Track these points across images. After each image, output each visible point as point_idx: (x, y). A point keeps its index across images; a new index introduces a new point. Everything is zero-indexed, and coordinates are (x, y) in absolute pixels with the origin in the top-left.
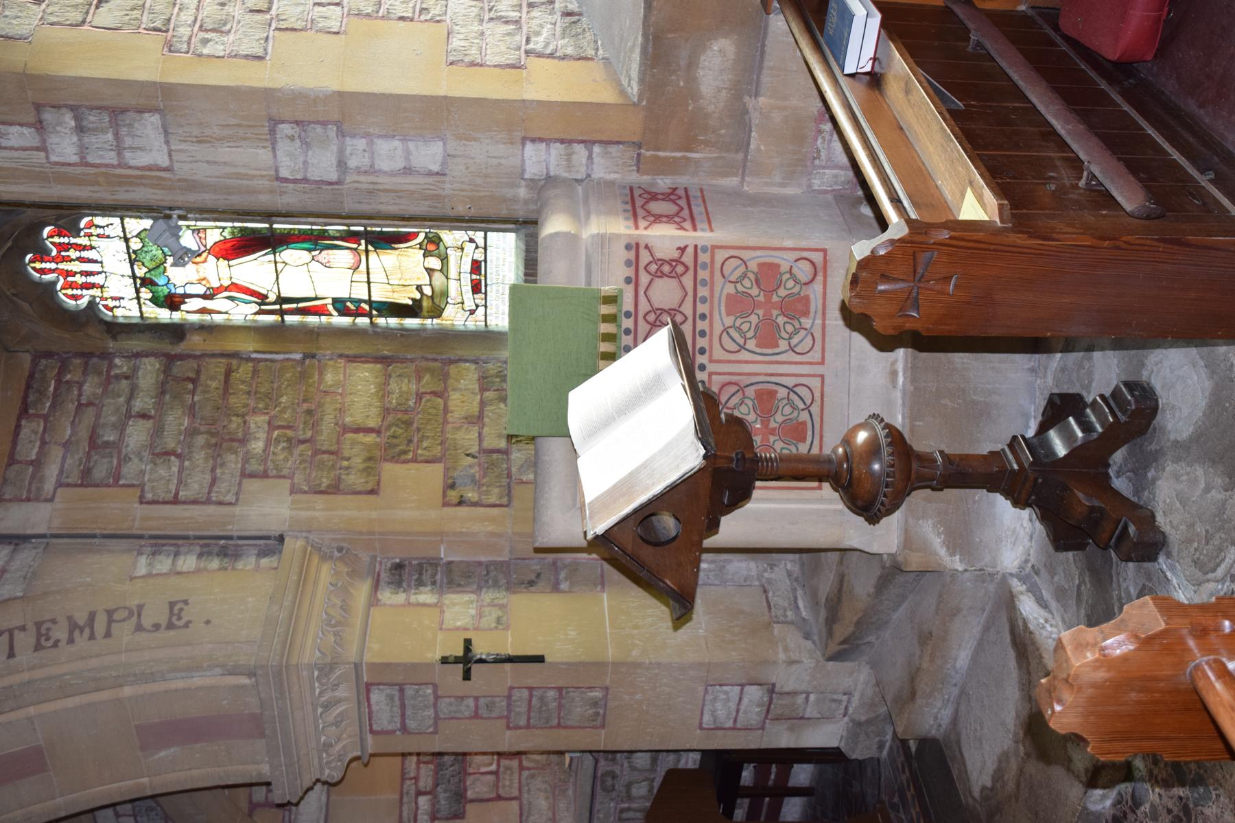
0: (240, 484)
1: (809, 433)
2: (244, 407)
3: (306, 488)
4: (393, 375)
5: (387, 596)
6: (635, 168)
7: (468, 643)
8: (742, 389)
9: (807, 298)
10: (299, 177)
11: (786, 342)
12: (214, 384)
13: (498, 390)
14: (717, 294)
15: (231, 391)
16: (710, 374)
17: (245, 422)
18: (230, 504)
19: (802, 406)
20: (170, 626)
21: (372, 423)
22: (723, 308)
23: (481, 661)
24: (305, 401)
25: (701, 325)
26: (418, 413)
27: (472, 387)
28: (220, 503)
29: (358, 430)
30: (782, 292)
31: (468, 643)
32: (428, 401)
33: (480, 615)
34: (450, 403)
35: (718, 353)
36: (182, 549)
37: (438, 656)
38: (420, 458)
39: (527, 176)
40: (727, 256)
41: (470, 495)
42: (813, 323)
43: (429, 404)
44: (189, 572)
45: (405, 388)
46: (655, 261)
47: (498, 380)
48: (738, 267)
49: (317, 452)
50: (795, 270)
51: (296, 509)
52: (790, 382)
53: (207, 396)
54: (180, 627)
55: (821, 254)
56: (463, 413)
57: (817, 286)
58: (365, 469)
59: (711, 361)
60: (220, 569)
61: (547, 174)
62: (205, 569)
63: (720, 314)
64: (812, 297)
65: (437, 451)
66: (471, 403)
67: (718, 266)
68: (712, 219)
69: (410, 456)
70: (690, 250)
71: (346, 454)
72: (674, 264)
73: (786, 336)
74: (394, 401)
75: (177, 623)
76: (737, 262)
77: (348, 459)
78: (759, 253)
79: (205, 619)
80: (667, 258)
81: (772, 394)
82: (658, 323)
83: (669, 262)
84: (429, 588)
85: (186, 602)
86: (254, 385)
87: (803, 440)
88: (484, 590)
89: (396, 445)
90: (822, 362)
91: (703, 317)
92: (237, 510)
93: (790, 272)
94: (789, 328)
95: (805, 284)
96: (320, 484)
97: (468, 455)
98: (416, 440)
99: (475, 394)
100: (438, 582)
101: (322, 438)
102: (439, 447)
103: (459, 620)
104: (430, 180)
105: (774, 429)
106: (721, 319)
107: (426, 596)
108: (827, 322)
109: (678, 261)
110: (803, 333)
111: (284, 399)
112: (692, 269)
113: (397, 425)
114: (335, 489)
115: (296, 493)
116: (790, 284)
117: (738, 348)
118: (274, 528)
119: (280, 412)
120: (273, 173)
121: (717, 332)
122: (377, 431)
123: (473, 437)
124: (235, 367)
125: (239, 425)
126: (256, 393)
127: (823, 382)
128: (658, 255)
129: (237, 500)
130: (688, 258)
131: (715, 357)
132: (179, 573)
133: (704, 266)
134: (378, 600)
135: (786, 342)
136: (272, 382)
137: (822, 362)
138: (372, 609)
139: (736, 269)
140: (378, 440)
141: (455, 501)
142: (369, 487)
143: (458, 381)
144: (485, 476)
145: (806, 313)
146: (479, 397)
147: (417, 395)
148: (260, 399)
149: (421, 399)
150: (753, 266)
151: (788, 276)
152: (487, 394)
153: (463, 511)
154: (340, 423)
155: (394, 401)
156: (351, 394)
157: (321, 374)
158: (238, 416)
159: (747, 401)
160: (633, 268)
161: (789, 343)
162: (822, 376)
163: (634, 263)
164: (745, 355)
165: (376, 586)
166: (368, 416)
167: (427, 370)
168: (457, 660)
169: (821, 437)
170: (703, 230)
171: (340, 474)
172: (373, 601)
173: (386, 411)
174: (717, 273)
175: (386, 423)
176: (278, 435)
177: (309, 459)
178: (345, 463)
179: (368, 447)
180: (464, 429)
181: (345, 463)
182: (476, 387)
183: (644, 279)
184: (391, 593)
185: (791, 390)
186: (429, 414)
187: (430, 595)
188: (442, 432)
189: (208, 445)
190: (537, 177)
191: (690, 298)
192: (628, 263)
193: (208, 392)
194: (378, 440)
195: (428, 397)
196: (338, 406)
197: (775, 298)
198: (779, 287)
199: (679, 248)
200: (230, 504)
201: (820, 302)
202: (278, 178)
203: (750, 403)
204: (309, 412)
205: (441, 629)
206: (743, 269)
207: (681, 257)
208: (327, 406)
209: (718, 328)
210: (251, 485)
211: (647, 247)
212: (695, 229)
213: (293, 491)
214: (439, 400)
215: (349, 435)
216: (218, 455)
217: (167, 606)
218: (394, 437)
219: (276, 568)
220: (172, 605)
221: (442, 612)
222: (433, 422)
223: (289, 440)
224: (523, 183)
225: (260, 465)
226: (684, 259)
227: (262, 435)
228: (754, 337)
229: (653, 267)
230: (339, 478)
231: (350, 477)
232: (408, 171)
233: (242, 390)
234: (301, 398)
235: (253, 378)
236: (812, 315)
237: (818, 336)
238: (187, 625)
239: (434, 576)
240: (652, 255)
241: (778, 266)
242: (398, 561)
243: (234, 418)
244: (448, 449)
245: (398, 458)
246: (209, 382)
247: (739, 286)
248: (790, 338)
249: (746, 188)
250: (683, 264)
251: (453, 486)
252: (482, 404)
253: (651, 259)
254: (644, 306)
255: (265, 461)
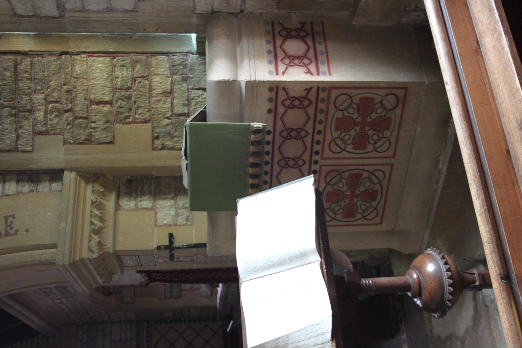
0: (33, 139)
1: (379, 196)
2: (28, 89)
3: (72, 141)
4: (117, 66)
5: (127, 203)
6: (276, 7)
7: (171, 236)
8: (340, 173)
9: (390, 119)
10: (31, 14)
11: (372, 146)
12: (8, 74)
13: (182, 74)
14: (330, 118)
15: (19, 78)
16: (321, 166)
17: (31, 99)
18: (30, 152)
19: (377, 181)
20: (7, 234)
21: (107, 98)
22: (333, 127)
23: (179, 248)
24: (65, 84)
25: (317, 137)
26: (134, 91)
27: (166, 73)
28: (24, 151)
29: (99, 103)
30: (374, 116)
31: (171, 236)
32: (140, 82)
33: (177, 215)
34: (153, 84)
35: (327, 153)
36: (7, 177)
37: (155, 246)
38: (138, 121)
39: (197, 12)
40: (339, 93)
41: (168, 143)
42: (391, 134)
43: (140, 85)
44: (13, 195)
45: (125, 75)
46: (289, 98)
47: (181, 67)
48: (346, 100)
49: (76, 118)
50: (384, 102)
51: (67, 154)
52: (371, 169)
53: (5, 82)
54: (12, 235)
55: (404, 91)
56: (161, 91)
57: (398, 112)
58: (105, 129)
59: (322, 158)
60: (30, 192)
61: (212, 10)
62: (22, 193)
63: (331, 130)
64: (393, 117)
65: (147, 116)
66: (166, 83)
67: (332, 100)
68: (330, 59)
69: (131, 119)
70: (314, 90)
71: (93, 119)
72: (302, 99)
73: (373, 142)
74: (119, 83)
75: (10, 231)
76: (345, 97)
77: (95, 122)
78: (361, 91)
79: (25, 229)
80: (298, 95)
81: (359, 176)
82: (289, 137)
83: (299, 99)
84: (148, 197)
85: (13, 216)
86: (33, 74)
87: (375, 200)
88: (179, 197)
89: (122, 113)
90: (394, 157)
91: (319, 132)
92: (34, 155)
93: (381, 103)
94: (375, 138)
95: (390, 110)
96: (80, 139)
97: (165, 118)
98: (134, 109)
99: (169, 77)
100: (153, 191)
101: (78, 109)
102: (148, 113)
103: (165, 219)
104: (127, 15)
105: (357, 195)
106: (331, 133)
107: (146, 202)
108: (401, 133)
109: (305, 98)
110: (384, 140)
111: (52, 83)
112: (314, 102)
113: (122, 100)
114: (88, 141)
115: (66, 144)
116: (380, 110)
117: (340, 150)
118: (57, 165)
119: (51, 92)
120: (11, 12)
121: (328, 141)
122: (110, 103)
123: (168, 106)
124: (19, 62)
125: (27, 101)
126: (35, 79)
127: (392, 168)
128: (292, 94)
129: (33, 149)
130: (312, 96)
131: (325, 156)
132: (7, 195)
133: (323, 100)
134: (120, 206)
135: (372, 146)
136: (44, 72)
137: (394, 157)
138: (117, 212)
139: (344, 102)
140: (111, 109)
141: (160, 147)
142: (108, 140)
143: (157, 68)
144: (176, 131)
145: (387, 128)
146: (170, 79)
147: (133, 79)
148: (38, 83)
149: (135, 81)
150: (356, 100)
151: (379, 105)
152: (175, 77)
153: (164, 152)
154: (88, 98)
155: (119, 83)
156: (92, 79)
157: (73, 65)
158: (26, 95)
159: (342, 180)
160: (274, 103)
161: (374, 147)
162: (392, 165)
163: (273, 100)
164: (345, 154)
165: (118, 197)
166: (104, 94)
167: (137, 61)
168: (166, 247)
169: (386, 197)
170: (324, 73)
171: (91, 132)
172: (118, 207)
173: (115, 89)
174: (332, 106)
175: (115, 98)
176: (52, 108)
177: (71, 122)
178: (93, 125)
179: (106, 114)
180: (162, 102)
181: (93, 125)
182: (168, 72)
183: (281, 110)
184: (127, 201)
185: (371, 173)
186: (141, 91)
187: (149, 202)
188: (149, 103)
189: (10, 115)
190: (204, 13)
191: (311, 122)
192: (270, 100)
193: (5, 80)
194: (111, 109)
195: (139, 80)
196: (86, 88)
197: (369, 120)
198: (372, 112)
199: (306, 89)
200: (30, 152)
201: (398, 121)
202: (15, 15)
203: (345, 181)
204: (68, 92)
205: (156, 226)
206: (349, 101)
207: (307, 95)
208: (79, 87)
209: (328, 139)
210: (40, 140)
211: (284, 89)
212: (318, 74)
213: (65, 142)
214: (147, 82)
215: (94, 107)
216: (18, 121)
217: (3, 220)
218: (121, 107)
219: (61, 191)
220: (6, 218)
221: (156, 213)
222: (143, 97)
223: (58, 111)
224: (194, 15)
225: (43, 127)
226: (309, 96)
227: (43, 108)
228: (352, 143)
229: (288, 102)
230: (91, 134)
231: (98, 134)
232: (109, 10)
233: (26, 77)
234: (62, 82)
235: (31, 69)
236: (391, 129)
237: (393, 141)
238: (16, 233)
239: (150, 188)
240: (287, 94)
241: (373, 99)
242: (129, 177)
243: (24, 97)
244: (153, 115)
245: (124, 121)
246: (5, 73)
247: (348, 142)
248: (375, 143)
249: (354, 23)
250: (308, 99)
251: (157, 138)
252: (172, 83)
253: (286, 97)
254: (280, 126)
255: (46, 124)
